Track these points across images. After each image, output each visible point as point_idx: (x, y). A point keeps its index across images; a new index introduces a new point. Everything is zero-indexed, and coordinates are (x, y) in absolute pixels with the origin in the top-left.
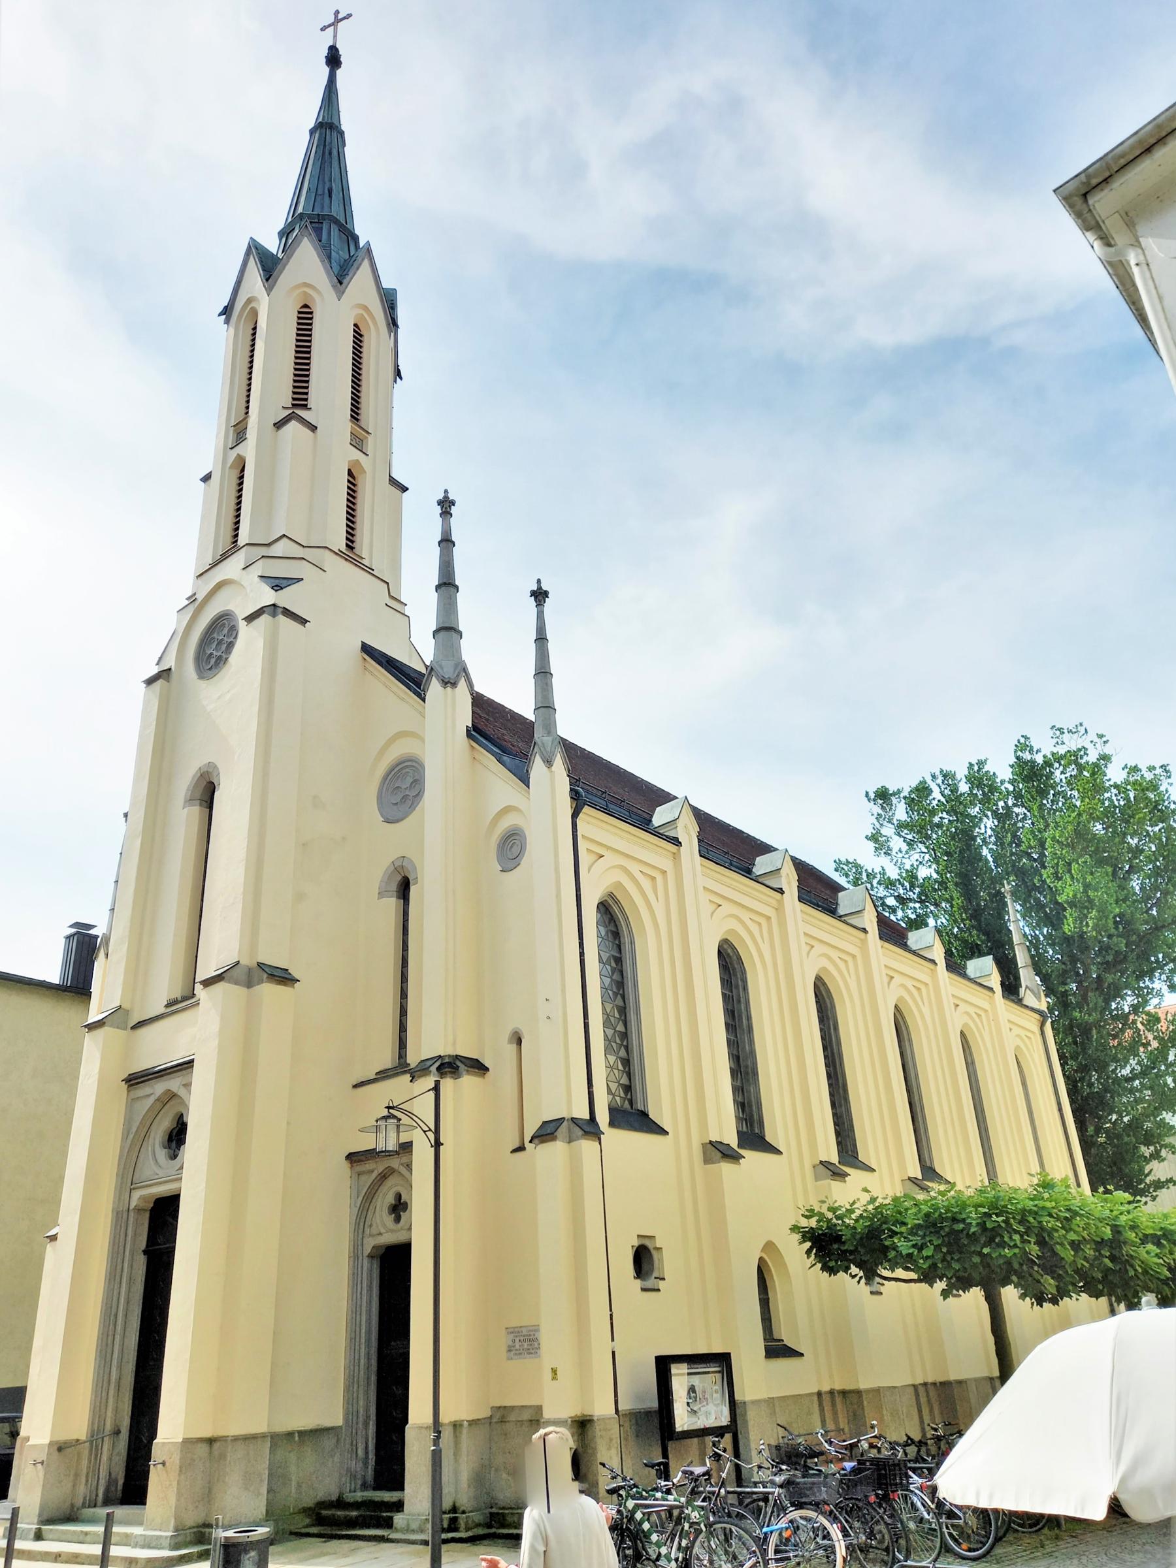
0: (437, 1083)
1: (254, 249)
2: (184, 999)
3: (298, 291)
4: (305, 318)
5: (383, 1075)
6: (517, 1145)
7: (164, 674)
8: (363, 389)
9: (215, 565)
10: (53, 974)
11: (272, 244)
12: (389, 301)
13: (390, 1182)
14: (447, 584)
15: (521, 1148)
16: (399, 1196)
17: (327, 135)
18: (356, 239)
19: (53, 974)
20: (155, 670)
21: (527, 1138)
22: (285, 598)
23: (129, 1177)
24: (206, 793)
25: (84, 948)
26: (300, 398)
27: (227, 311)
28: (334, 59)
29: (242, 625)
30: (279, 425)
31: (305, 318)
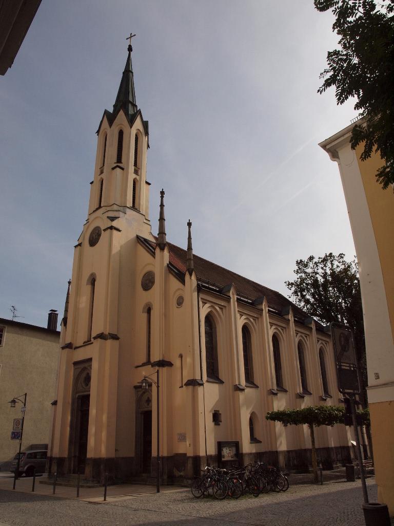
0: (158, 370)
1: (106, 112)
2: (88, 341)
3: (119, 127)
4: (121, 133)
5: (144, 365)
6: (181, 386)
7: (80, 245)
8: (138, 145)
9: (94, 211)
10: (44, 325)
11: (111, 110)
12: (145, 125)
13: (146, 394)
14: (162, 219)
15: (182, 387)
16: (148, 398)
17: (127, 74)
18: (136, 106)
19: (44, 325)
20: (77, 243)
21: (183, 384)
22: (115, 224)
23: (75, 390)
24: (93, 281)
25: (53, 316)
26: (119, 159)
27: (98, 132)
28: (130, 49)
29: (103, 231)
30: (113, 169)
31: (121, 133)
